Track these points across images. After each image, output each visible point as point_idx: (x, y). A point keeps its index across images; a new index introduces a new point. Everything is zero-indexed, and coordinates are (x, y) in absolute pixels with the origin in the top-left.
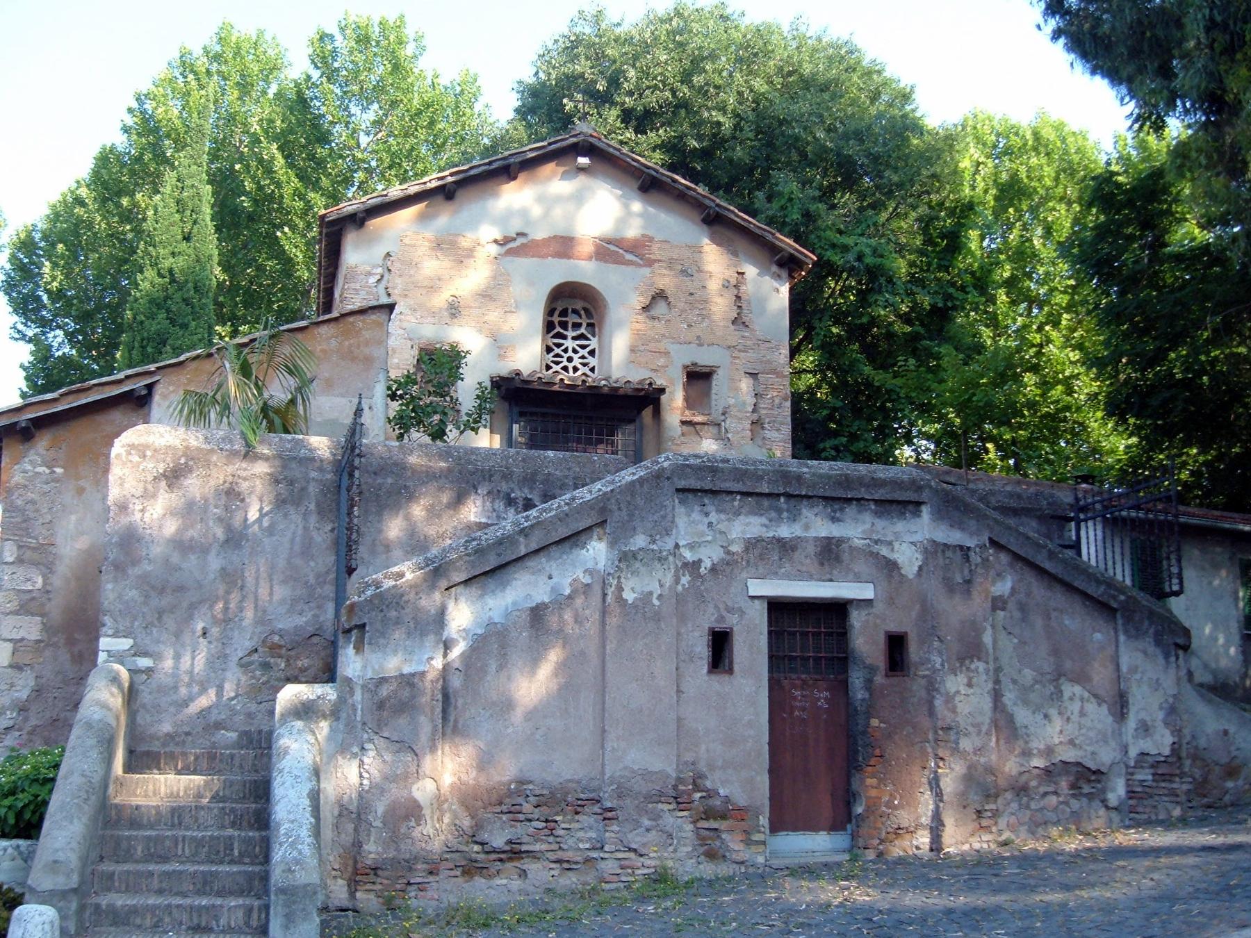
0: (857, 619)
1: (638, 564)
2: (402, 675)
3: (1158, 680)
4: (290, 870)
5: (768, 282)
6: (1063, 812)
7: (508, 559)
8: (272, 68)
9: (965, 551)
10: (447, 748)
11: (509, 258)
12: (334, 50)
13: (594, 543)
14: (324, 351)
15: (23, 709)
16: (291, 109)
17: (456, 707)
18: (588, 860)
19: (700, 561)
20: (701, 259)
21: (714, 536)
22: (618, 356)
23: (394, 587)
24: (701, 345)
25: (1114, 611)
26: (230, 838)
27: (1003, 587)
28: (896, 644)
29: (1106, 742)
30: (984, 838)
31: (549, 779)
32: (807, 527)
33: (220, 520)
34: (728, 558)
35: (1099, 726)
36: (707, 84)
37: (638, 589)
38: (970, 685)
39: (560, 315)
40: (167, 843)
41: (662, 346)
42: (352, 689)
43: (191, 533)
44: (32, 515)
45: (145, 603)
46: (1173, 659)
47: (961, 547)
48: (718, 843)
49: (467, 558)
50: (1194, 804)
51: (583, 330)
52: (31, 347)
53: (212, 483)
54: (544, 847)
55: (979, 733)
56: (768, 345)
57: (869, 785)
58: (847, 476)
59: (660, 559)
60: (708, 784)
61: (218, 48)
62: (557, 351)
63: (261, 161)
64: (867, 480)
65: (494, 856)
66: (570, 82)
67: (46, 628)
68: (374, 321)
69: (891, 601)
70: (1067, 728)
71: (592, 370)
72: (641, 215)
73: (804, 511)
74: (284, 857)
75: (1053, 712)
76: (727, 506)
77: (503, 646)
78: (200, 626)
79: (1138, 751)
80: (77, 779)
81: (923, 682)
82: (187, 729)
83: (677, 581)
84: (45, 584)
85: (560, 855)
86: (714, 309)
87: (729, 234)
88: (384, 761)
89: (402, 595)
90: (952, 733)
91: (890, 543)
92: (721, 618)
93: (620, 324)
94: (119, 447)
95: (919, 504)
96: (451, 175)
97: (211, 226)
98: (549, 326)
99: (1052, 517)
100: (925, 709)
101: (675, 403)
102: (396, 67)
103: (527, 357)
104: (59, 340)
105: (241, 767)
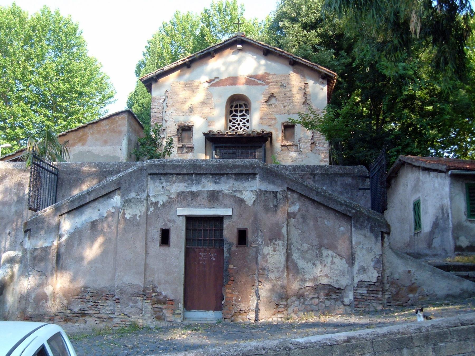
0: (226, 223)
1: (131, 204)
2: (42, 247)
5: (319, 86)
6: (321, 306)
7: (82, 204)
9: (275, 194)
10: (59, 274)
11: (212, 88)
13: (116, 196)
14: (104, 130)
17: (62, 259)
18: (110, 318)
19: (158, 202)
20: (289, 80)
21: (164, 192)
22: (255, 122)
27: (295, 208)
28: (242, 236)
30: (279, 316)
31: (96, 286)
32: (204, 187)
33: (16, 194)
34: (170, 200)
35: (341, 269)
37: (131, 213)
38: (274, 251)
39: (235, 108)
41: (273, 116)
42: (27, 252)
43: (7, 199)
46: (380, 238)
47: (273, 192)
48: (162, 314)
49: (67, 204)
50: (391, 304)
53: (13, 181)
54: (93, 312)
55: (278, 271)
57: (228, 292)
59: (140, 202)
60: (158, 290)
62: (234, 121)
65: (75, 315)
68: (122, 117)
69: (240, 216)
70: (325, 270)
71: (248, 128)
72: (265, 65)
73: (203, 180)
75: (317, 262)
76: (170, 180)
77: (80, 236)
78: (8, 231)
79: (359, 280)
81: (254, 249)
83: (148, 210)
85: (99, 315)
86: (295, 99)
87: (301, 68)
88: (36, 279)
89: (44, 218)
90: (266, 271)
91: (241, 192)
92: (166, 224)
93: (256, 109)
100: (254, 261)
101: (279, 139)
103: (219, 126)
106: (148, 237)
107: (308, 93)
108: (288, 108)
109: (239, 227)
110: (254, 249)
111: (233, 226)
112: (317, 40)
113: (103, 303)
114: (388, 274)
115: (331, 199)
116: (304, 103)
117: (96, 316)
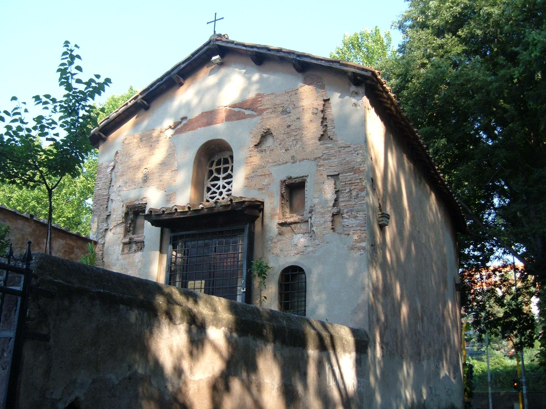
62: (214, 189)
87: (318, 74)
101: (274, 211)
103: (184, 199)
107: (329, 117)
108: (292, 152)
112: (459, 49)
116: (322, 138)
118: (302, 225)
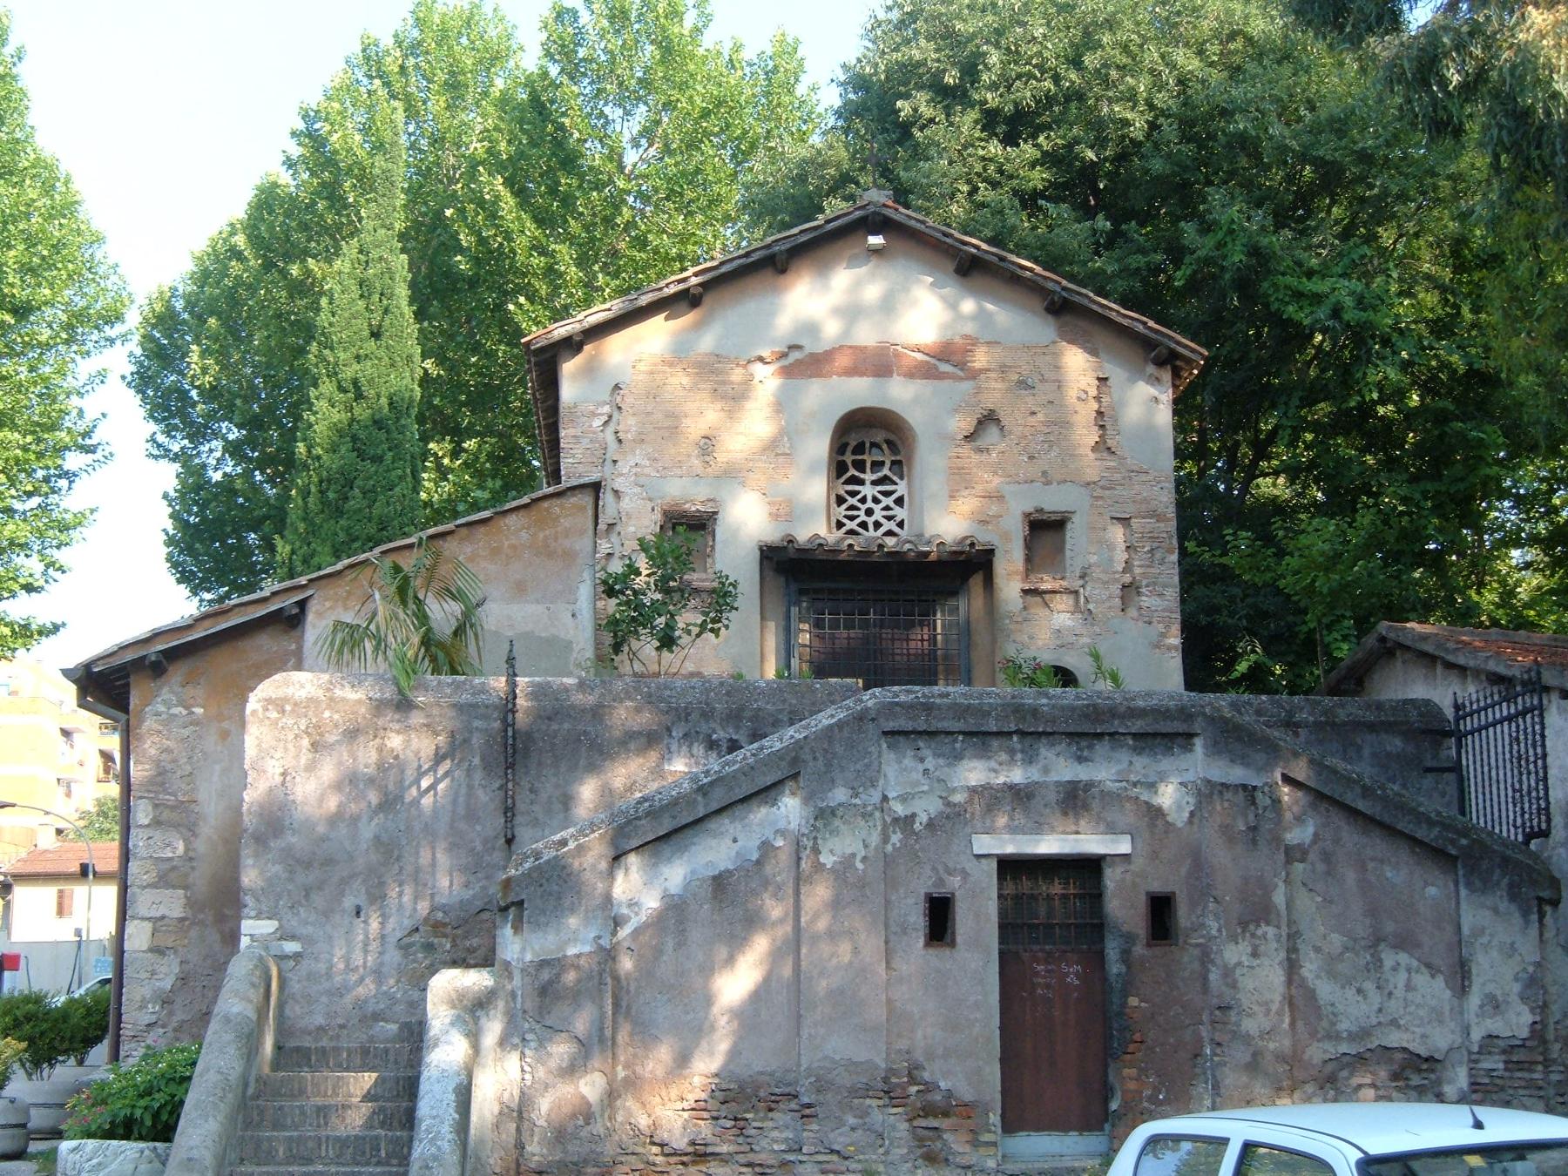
0: (1112, 878)
3: (1512, 944)
4: (427, 1167)
5: (1144, 390)
8: (494, 58)
12: (580, 31)
14: (514, 547)
15: (166, 1001)
16: (521, 122)
17: (628, 992)
19: (914, 815)
23: (556, 857)
24: (1048, 483)
25: (1453, 860)
26: (377, 1138)
28: (1161, 909)
29: (1441, 1022)
32: (1046, 770)
35: (1433, 1003)
36: (1105, 65)
37: (838, 851)
39: (854, 452)
40: (310, 1144)
44: (169, 767)
45: (291, 880)
46: (1535, 917)
47: (1244, 787)
48: (939, 1145)
51: (886, 471)
52: (177, 467)
54: (732, 1148)
56: (1143, 477)
58: (1095, 706)
59: (864, 815)
60: (926, 1076)
61: (416, 33)
63: (481, 203)
64: (1122, 709)
65: (673, 1160)
66: (906, 76)
67: (190, 903)
69: (1154, 855)
71: (901, 524)
73: (1043, 751)
74: (422, 1153)
79: (1484, 1033)
80: (212, 1077)
81: (1196, 952)
82: (340, 1021)
83: (886, 839)
84: (187, 850)
85: (751, 1157)
92: (941, 882)
94: (254, 702)
95: (1190, 736)
96: (696, 274)
97: (408, 311)
98: (839, 469)
99: (1423, 732)
102: (667, 50)
104: (218, 454)
105: (396, 1062)
106: (891, 922)
109: (1151, 889)
110: (1196, 952)
111: (1134, 884)
113: (762, 1120)
114: (1558, 1016)
115: (1402, 807)
117: (742, 1159)
118: (1065, 597)
